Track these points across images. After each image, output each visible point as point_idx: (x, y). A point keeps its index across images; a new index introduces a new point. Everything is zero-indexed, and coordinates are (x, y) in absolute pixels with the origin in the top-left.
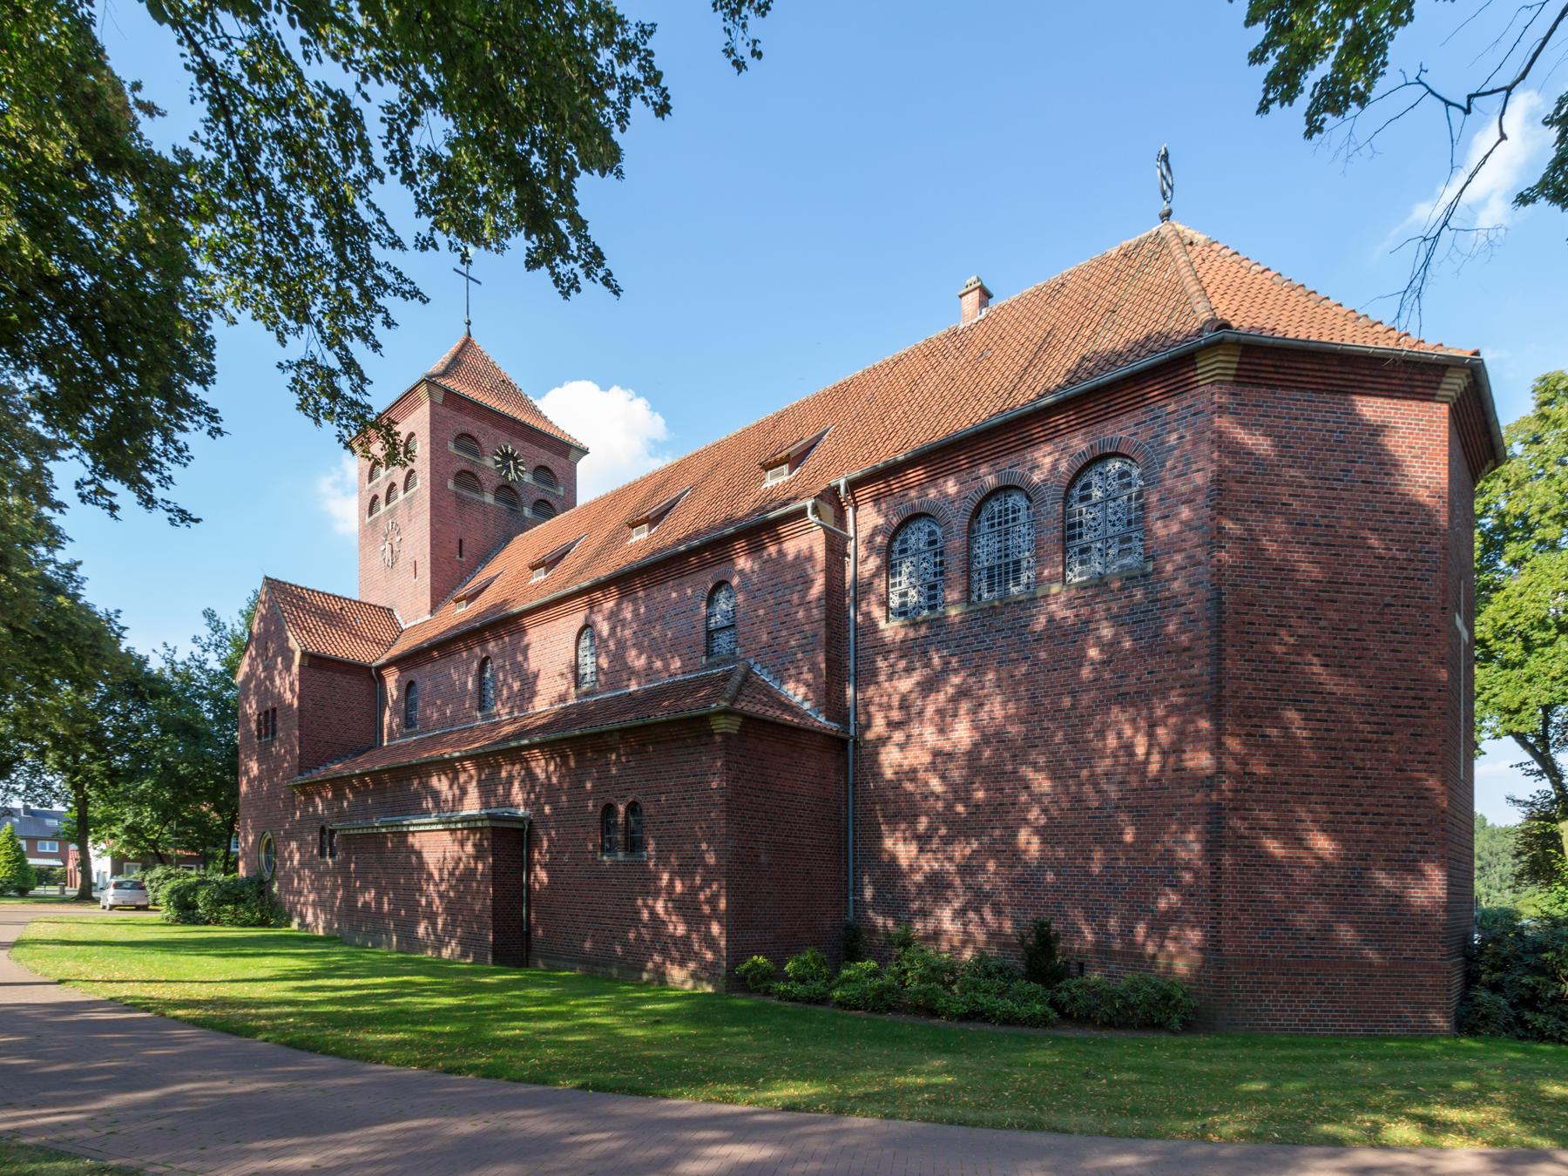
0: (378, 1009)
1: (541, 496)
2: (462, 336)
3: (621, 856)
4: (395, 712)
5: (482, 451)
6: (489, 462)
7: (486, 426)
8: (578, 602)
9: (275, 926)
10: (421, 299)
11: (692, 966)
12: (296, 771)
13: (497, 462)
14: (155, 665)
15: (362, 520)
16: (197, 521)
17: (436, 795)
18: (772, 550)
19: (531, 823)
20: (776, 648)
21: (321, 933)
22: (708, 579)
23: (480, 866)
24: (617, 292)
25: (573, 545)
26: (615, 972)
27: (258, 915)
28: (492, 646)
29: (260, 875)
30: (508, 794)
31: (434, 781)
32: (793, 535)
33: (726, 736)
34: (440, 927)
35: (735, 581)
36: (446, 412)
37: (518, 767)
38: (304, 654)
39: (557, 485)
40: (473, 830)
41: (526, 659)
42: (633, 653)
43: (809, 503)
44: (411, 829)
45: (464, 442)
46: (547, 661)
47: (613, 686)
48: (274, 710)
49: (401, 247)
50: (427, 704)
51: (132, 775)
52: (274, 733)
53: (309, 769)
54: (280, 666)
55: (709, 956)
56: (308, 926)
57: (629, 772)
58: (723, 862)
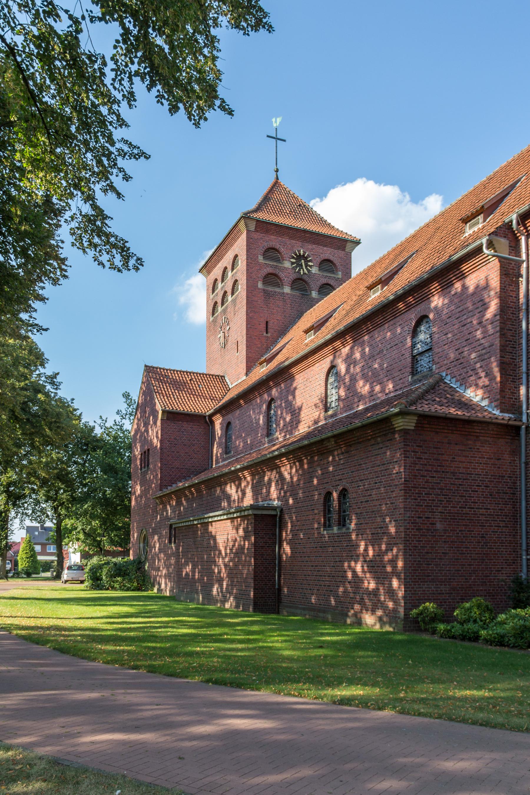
0: (141, 634)
1: (324, 281)
2: (273, 180)
3: (335, 529)
4: (219, 445)
5: (282, 258)
6: (287, 264)
7: (286, 239)
8: (326, 350)
9: (144, 590)
10: (145, 157)
11: (379, 613)
12: (159, 488)
13: (293, 263)
14: (98, 431)
15: (208, 319)
16: (46, 330)
17: (228, 497)
18: (458, 286)
19: (282, 511)
20: (462, 360)
21: (168, 595)
22: (413, 316)
23: (247, 543)
24: (230, 113)
25: (335, 310)
26: (329, 617)
27: (135, 584)
28: (274, 392)
29: (139, 558)
30: (269, 492)
31: (228, 488)
32: (474, 269)
33: (405, 432)
34: (225, 586)
35: (431, 316)
36: (257, 236)
37: (274, 472)
38: (164, 412)
39: (337, 271)
40: (243, 517)
41: (294, 397)
42: (361, 383)
43: (484, 241)
44: (210, 520)
45: (270, 254)
46: (308, 396)
47: (348, 407)
48: (148, 450)
49: (126, 125)
50: (237, 438)
51: (82, 500)
52: (148, 466)
53: (166, 487)
54: (151, 422)
55: (391, 605)
56: (162, 590)
57: (341, 467)
58: (402, 529)
